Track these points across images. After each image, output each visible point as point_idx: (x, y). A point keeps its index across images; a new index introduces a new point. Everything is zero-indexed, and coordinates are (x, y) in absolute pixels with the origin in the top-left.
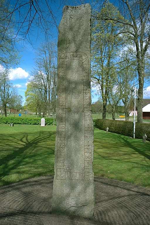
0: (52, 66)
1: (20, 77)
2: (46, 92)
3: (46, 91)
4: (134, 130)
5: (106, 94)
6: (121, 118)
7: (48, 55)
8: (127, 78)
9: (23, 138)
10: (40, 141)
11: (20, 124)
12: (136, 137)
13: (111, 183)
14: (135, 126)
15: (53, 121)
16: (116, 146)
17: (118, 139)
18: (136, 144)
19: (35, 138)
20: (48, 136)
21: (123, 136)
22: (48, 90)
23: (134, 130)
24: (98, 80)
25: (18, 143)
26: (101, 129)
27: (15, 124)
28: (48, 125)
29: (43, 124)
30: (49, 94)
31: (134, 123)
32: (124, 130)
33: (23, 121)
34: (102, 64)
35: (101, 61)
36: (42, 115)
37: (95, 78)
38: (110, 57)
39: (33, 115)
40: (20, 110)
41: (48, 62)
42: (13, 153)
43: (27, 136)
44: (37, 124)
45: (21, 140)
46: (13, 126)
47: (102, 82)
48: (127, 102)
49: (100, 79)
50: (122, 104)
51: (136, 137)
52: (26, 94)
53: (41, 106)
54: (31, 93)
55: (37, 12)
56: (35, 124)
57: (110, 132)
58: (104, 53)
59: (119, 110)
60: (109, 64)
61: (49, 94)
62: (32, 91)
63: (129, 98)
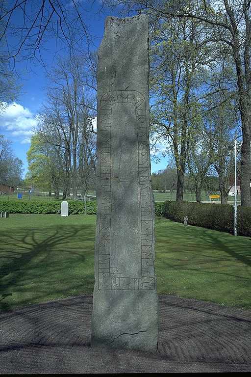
0: (79, 101)
1: (21, 121)
2: (69, 151)
3: (68, 150)
4: (236, 220)
5: (182, 156)
6: (213, 199)
7: (71, 81)
8: (222, 124)
9: (26, 236)
10: (57, 241)
11: (20, 213)
12: (239, 234)
13: (187, 305)
14: (236, 213)
15: (83, 207)
16: (197, 247)
17: (202, 237)
18: (232, 244)
19: (49, 237)
20: (72, 234)
21: (210, 232)
22: (72, 147)
23: (236, 220)
24: (168, 129)
25: (17, 245)
26: (173, 219)
27: (11, 213)
28: (75, 214)
29: (64, 213)
30: (75, 155)
31: (235, 207)
32: (216, 221)
33: (26, 207)
34: (174, 98)
35: (172, 93)
36: (61, 196)
37: (161, 124)
38: (188, 86)
39: (44, 196)
40: (16, 187)
41: (72, 93)
42: (22, 257)
43: (33, 234)
44: (53, 213)
45: (23, 241)
46: (7, 217)
47: (175, 131)
48: (224, 168)
49: (171, 127)
50: (215, 174)
51: (239, 234)
52: (30, 156)
53: (58, 179)
54: (38, 154)
55: (54, 10)
56: (49, 213)
57: (191, 225)
58: (178, 78)
59: (204, 183)
60: (186, 98)
61: (75, 155)
62: (42, 150)
63: (226, 162)
